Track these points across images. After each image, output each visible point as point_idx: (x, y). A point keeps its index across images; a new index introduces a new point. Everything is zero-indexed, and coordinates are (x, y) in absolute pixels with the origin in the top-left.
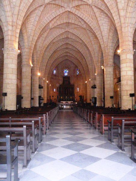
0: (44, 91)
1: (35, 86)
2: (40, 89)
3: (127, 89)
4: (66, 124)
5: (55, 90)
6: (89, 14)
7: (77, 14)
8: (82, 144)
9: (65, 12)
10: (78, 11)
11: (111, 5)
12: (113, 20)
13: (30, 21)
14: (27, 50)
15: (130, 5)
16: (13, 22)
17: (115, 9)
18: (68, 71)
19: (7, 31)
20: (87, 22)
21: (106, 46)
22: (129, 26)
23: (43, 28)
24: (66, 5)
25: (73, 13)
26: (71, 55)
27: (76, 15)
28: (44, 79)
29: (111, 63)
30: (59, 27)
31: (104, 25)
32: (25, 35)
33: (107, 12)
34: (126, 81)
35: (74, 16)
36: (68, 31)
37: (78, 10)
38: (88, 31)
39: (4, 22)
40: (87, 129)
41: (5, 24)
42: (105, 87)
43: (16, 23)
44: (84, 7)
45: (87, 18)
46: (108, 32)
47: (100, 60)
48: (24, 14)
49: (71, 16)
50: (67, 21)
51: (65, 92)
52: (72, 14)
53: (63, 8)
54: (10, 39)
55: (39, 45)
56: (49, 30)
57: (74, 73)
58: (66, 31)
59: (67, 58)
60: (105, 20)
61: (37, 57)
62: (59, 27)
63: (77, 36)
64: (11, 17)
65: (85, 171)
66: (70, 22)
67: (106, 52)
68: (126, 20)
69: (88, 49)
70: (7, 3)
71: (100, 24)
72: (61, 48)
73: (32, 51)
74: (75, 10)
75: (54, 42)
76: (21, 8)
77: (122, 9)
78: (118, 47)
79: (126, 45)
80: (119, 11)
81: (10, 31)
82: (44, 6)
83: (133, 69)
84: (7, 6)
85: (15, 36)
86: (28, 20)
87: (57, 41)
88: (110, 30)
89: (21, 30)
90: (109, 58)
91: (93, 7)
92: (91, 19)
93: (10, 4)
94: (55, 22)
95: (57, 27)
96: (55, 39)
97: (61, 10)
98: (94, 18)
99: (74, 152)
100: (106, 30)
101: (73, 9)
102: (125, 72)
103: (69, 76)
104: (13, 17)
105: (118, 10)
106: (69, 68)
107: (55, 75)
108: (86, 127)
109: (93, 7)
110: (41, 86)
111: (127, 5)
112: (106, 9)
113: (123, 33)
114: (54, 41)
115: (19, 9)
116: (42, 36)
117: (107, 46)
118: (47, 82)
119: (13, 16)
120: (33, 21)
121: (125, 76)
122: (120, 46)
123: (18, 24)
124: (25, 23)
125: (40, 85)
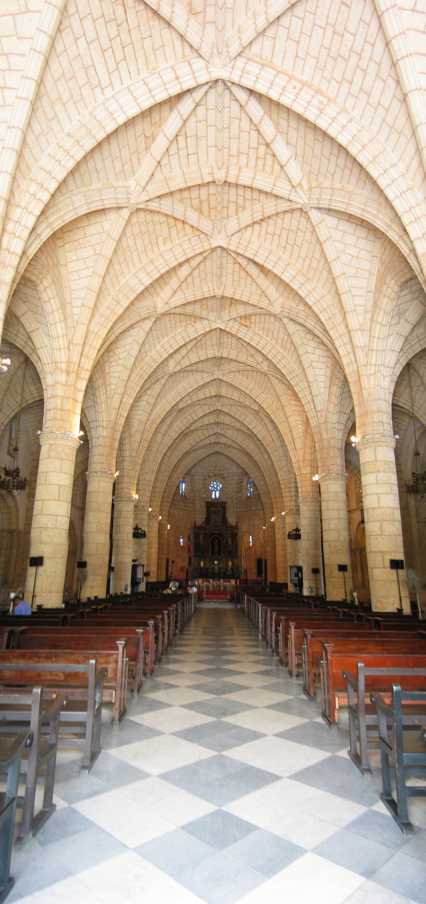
0: (149, 544)
2: (136, 540)
4: (206, 646)
5: (181, 540)
6: (275, 336)
7: (242, 337)
8: (235, 727)
9: (211, 331)
10: (246, 329)
11: (330, 318)
12: (336, 356)
13: (116, 357)
14: (105, 430)
15: (380, 320)
16: (69, 362)
17: (342, 329)
18: (221, 486)
19: (52, 386)
20: (269, 357)
21: (322, 421)
22: (379, 371)
23: (149, 373)
24: (212, 316)
25: (232, 334)
26: (229, 442)
27: (240, 338)
28: (150, 510)
29: (339, 468)
30: (194, 368)
31: (315, 364)
32: (101, 392)
33: (320, 335)
34: (377, 524)
35: (234, 341)
37: (247, 326)
38: (275, 382)
39: (46, 363)
41: (47, 369)
42: (325, 538)
43: (77, 365)
45: (269, 347)
46: (328, 383)
47: (308, 457)
48: (100, 342)
49: (226, 339)
50: (217, 354)
51: (213, 545)
52: (230, 336)
53: (205, 322)
54: (59, 406)
55: (138, 417)
56: (166, 377)
58: (215, 380)
59: (217, 449)
60: (318, 352)
62: (194, 368)
63: (244, 392)
64: (66, 350)
65: (227, 815)
66: (225, 355)
67: (322, 439)
68: (371, 358)
69: (276, 428)
71: (306, 365)
72: (200, 424)
73: (118, 436)
76: (92, 327)
77: (360, 329)
78: (352, 431)
79: (373, 422)
80: (352, 333)
81: (59, 385)
82: (153, 319)
83: (396, 490)
84: (59, 325)
86: (111, 354)
88: (331, 381)
89: (91, 380)
91: (285, 321)
92: (281, 351)
93: (65, 319)
94: (183, 358)
95: (190, 368)
96: (185, 400)
98: (288, 347)
99: (207, 753)
100: (323, 380)
101: (231, 323)
102: (375, 497)
103: (223, 500)
104: (69, 350)
105: (349, 332)
106: (223, 478)
107: (184, 497)
108: (262, 668)
109: (285, 321)
110: (140, 531)
111: (372, 319)
112: (317, 327)
113: (363, 390)
114: (181, 406)
115: (88, 331)
116: (149, 392)
117: (326, 422)
119: (71, 348)
121: (374, 509)
122: (357, 425)
123: (83, 368)
124: (101, 361)
125: (136, 528)
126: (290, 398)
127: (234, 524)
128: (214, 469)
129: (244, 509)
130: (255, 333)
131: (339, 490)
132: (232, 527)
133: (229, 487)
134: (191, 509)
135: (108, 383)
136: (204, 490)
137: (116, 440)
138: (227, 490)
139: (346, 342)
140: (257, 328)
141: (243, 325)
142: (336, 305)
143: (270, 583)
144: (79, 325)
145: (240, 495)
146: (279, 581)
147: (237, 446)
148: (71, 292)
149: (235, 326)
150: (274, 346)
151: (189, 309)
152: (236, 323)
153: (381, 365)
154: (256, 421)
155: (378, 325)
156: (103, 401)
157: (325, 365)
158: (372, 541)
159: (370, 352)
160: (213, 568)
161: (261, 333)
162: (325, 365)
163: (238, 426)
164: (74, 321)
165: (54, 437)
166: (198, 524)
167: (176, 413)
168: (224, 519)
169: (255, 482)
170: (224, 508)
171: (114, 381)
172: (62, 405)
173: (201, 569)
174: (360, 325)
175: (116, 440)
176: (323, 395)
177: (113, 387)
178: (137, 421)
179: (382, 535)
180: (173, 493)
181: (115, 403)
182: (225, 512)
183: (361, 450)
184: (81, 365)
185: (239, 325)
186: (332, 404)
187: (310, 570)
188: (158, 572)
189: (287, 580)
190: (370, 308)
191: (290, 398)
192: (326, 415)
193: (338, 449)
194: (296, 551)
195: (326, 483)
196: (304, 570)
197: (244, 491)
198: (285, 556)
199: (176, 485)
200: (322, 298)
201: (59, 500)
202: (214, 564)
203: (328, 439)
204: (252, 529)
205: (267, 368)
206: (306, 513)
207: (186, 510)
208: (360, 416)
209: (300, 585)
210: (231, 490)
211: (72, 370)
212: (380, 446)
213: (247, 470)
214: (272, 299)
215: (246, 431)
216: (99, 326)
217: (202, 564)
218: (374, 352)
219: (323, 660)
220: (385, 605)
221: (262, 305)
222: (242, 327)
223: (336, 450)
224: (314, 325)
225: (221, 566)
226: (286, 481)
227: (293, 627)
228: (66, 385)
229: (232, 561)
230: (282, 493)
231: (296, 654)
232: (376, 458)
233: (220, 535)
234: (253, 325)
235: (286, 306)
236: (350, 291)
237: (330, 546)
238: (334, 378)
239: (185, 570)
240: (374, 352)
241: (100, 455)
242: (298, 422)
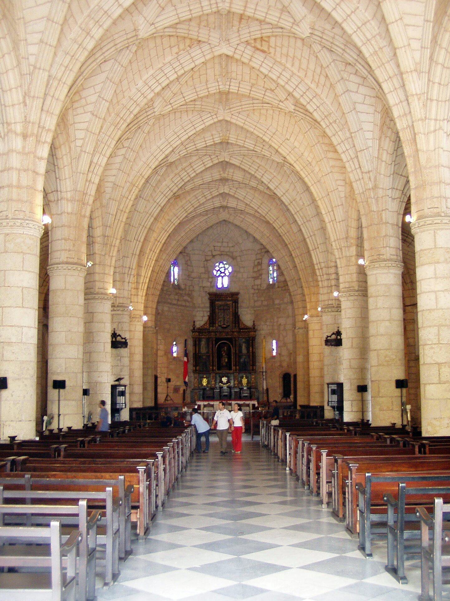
0: (131, 355)
1: (96, 340)
3: (440, 360)
5: (175, 349)
6: (304, 66)
10: (263, 55)
11: (376, 52)
13: (83, 102)
16: (26, 121)
17: (391, 68)
18: (230, 269)
21: (370, 186)
22: (440, 128)
24: (215, 37)
26: (241, 206)
29: (393, 251)
31: (359, 107)
34: (434, 330)
36: (227, 121)
37: (263, 51)
40: (284, 503)
43: (37, 126)
44: (286, 43)
46: (377, 134)
54: (15, 183)
55: (112, 179)
57: (256, 278)
58: (220, 121)
59: (224, 215)
60: (362, 90)
61: (105, 226)
70: (12, 82)
72: (198, 181)
74: (250, 53)
75: (172, 163)
77: (416, 70)
79: (433, 197)
80: (404, 76)
81: (14, 154)
84: (11, 74)
85: (34, 172)
87: (184, 157)
90: (384, 234)
92: (313, 86)
93: (19, 64)
97: (196, 52)
100: (371, 129)
102: (433, 296)
103: (234, 290)
105: (401, 74)
106: (234, 258)
110: (119, 339)
111: (431, 58)
113: (420, 153)
117: (375, 187)
118: (145, 318)
119: (28, 102)
120: (93, 98)
121: (430, 310)
122: (413, 200)
123: (44, 127)
125: (114, 335)
126: (326, 148)
127: (249, 324)
128: (219, 244)
129: (265, 303)
130: (276, 61)
131: (392, 282)
132: (247, 328)
133: (242, 270)
134: (188, 304)
135: (72, 139)
136: (206, 276)
137: (84, 216)
138: (240, 275)
139: (397, 86)
140: (278, 55)
141: (258, 49)
142: (384, 35)
143: (301, 406)
144: (37, 71)
145: (258, 282)
146: (312, 404)
147: (252, 212)
148: (25, 23)
149: (246, 51)
150: (302, 80)
151: (182, 30)
152: (249, 47)
153: (444, 120)
154: (279, 177)
155: (439, 67)
156: (66, 164)
157: (374, 108)
158: (426, 352)
159: (429, 102)
160: (221, 388)
161: (283, 61)
162: (374, 108)
163: (253, 183)
164: (29, 65)
165: (10, 224)
166: (199, 324)
167: (164, 169)
168: (236, 317)
169: (280, 263)
170: (236, 302)
171: (80, 134)
172: (19, 180)
173: (204, 389)
174: (416, 64)
175: (84, 216)
176: (370, 149)
177: (79, 143)
178: (110, 185)
179: (439, 343)
180: (162, 282)
181: (84, 165)
182: (236, 307)
183: (417, 233)
184: (41, 124)
185: (253, 49)
186: (384, 164)
187: (355, 387)
188: (143, 394)
189: (323, 402)
190: (428, 42)
191: (326, 148)
192: (375, 178)
193: (393, 225)
194: (336, 362)
195: (375, 272)
196: (346, 388)
197: (264, 276)
198: (322, 369)
199: (166, 271)
200: (364, 24)
201: (23, 307)
202: (221, 382)
203: (378, 211)
204: (276, 331)
205: (293, 107)
206: (349, 311)
207: (181, 306)
208: (416, 188)
209: (340, 408)
210: (245, 275)
211: (29, 133)
212: (442, 229)
213: (268, 247)
214: (298, 17)
215: (265, 191)
216: (63, 69)
217: (205, 382)
218: (434, 103)
219: (348, 480)
220: (437, 428)
221: (283, 23)
222: (258, 52)
223: (390, 226)
224: (356, 57)
225: (232, 384)
226: (323, 265)
227: (324, 454)
228: (23, 153)
229: (247, 378)
230: (317, 281)
231: (327, 482)
232: (435, 246)
233: (230, 340)
234: (272, 50)
235: (316, 27)
236: (401, 19)
237: (378, 356)
238: (385, 128)
239: (181, 391)
240: (434, 103)
241: (65, 240)
242: (339, 182)
